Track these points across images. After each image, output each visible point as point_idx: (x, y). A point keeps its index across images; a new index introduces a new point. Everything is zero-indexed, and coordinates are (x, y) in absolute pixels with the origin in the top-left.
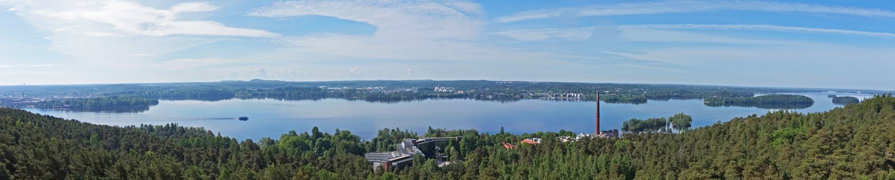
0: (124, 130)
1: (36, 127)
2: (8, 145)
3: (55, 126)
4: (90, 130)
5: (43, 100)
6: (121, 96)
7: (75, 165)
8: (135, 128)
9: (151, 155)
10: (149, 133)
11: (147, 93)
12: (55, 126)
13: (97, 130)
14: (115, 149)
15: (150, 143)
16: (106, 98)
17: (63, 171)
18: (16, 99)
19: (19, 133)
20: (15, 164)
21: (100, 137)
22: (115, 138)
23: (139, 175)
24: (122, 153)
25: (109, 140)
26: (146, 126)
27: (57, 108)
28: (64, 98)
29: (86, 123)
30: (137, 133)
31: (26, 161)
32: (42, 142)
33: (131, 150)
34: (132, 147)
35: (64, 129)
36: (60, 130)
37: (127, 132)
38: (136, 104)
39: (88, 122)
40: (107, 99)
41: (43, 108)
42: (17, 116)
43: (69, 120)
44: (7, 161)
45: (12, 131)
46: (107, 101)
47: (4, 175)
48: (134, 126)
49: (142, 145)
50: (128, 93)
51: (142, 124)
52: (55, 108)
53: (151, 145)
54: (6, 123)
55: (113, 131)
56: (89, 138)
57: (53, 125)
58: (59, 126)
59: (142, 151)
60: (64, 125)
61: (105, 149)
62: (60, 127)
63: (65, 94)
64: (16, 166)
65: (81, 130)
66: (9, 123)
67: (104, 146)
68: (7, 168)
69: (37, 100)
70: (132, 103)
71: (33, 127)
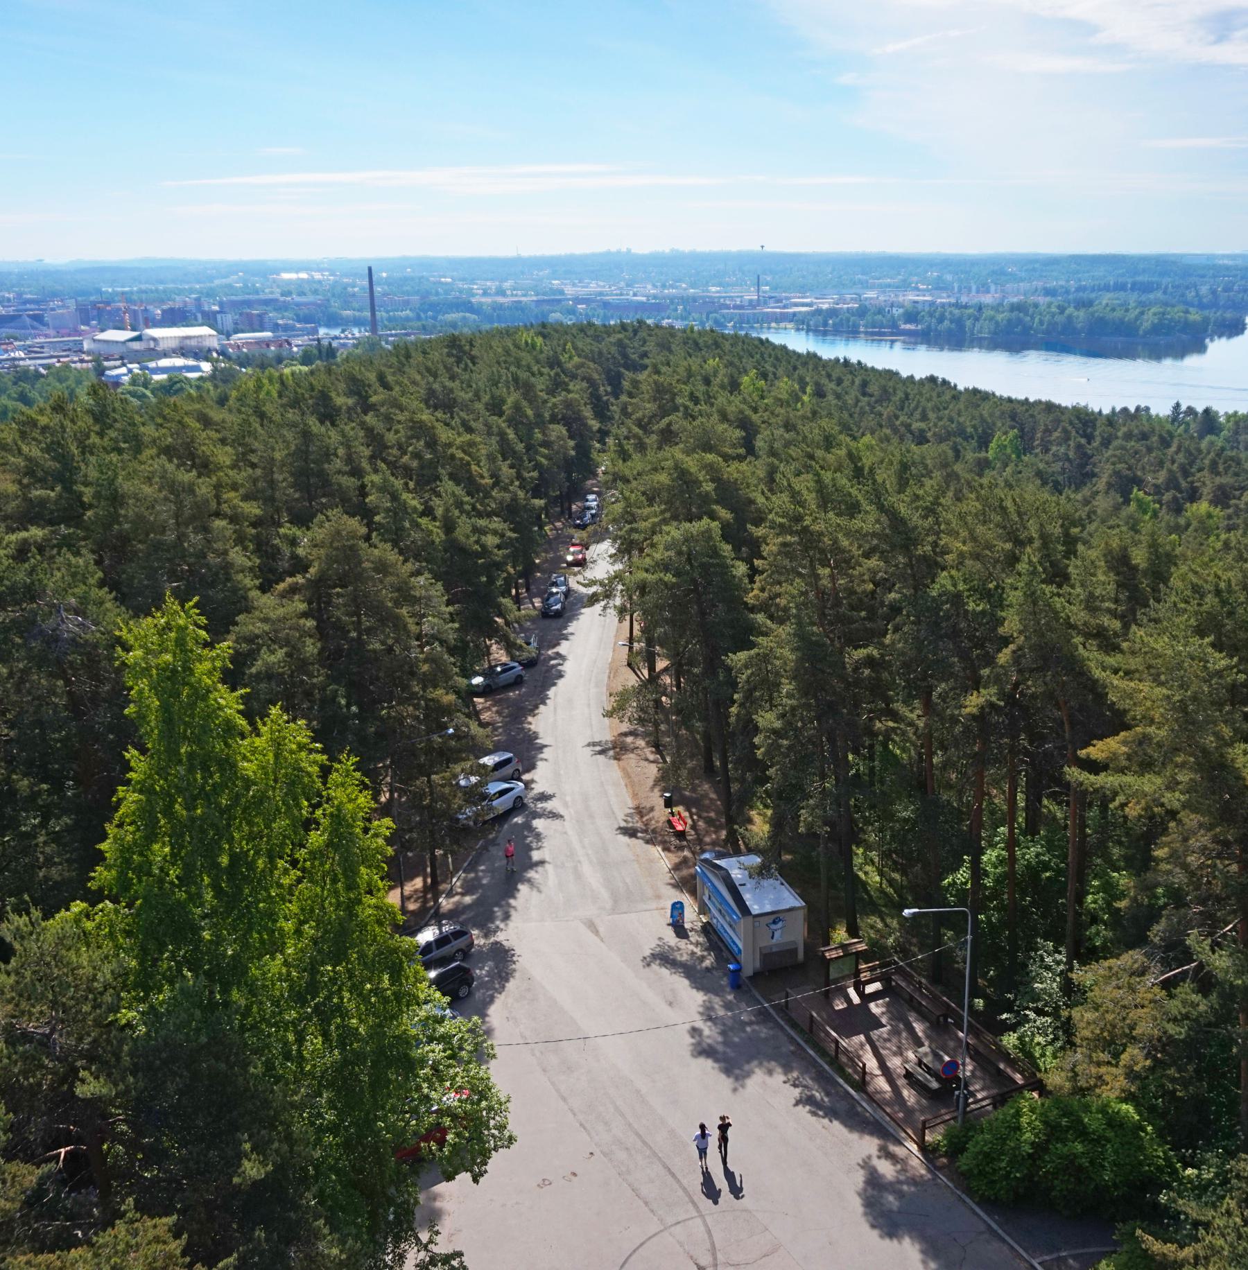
0: (1112, 420)
1: (806, 398)
2: (727, 458)
3: (871, 396)
4: (991, 415)
5: (825, 307)
6: (1106, 298)
7: (974, 539)
8: (1150, 417)
9: (1210, 516)
10: (1201, 437)
11: (1204, 290)
12: (871, 396)
13: (1013, 417)
14: (1077, 490)
15: (1206, 473)
16: (1049, 305)
17: (925, 558)
18: (731, 298)
19: (755, 418)
20: (757, 526)
21: (1025, 443)
22: (1079, 447)
23: (1218, 592)
24: (1103, 504)
25: (1054, 455)
26: (1191, 411)
27: (873, 334)
28: (901, 299)
29: (975, 391)
30: (1161, 436)
31: (798, 519)
32: (842, 452)
33: (1136, 493)
34: (1139, 482)
35: (902, 409)
36: (887, 410)
37: (1124, 429)
38: (1156, 329)
39: (984, 386)
40: (1054, 309)
41: (825, 333)
42: (740, 358)
43: (917, 377)
44: (725, 514)
45: (731, 409)
46: (1053, 315)
47: (714, 561)
48: (1147, 409)
49: (1176, 479)
50: (1133, 289)
51: (1178, 405)
52: (866, 333)
53: (1208, 483)
54: (707, 381)
55: (1071, 423)
56: (984, 443)
57: (864, 394)
58: (885, 395)
59: (1175, 499)
60: (900, 395)
61: (1044, 483)
62: (890, 400)
63: (905, 286)
64: (759, 532)
65: (959, 415)
66: (716, 381)
67: (1039, 474)
68: (726, 537)
69: (803, 305)
70: (1146, 325)
71: (798, 399)
